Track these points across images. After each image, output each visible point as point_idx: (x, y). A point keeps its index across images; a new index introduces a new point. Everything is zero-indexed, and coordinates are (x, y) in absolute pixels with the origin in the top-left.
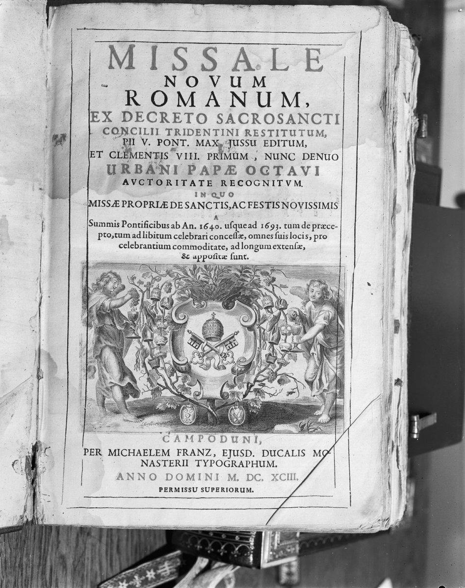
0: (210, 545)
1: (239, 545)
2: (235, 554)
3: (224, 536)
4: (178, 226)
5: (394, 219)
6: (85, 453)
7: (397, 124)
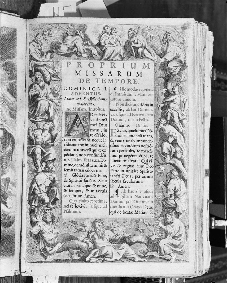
4: (134, 141)
5: (204, 122)
6: (68, 66)
7: (205, 75)
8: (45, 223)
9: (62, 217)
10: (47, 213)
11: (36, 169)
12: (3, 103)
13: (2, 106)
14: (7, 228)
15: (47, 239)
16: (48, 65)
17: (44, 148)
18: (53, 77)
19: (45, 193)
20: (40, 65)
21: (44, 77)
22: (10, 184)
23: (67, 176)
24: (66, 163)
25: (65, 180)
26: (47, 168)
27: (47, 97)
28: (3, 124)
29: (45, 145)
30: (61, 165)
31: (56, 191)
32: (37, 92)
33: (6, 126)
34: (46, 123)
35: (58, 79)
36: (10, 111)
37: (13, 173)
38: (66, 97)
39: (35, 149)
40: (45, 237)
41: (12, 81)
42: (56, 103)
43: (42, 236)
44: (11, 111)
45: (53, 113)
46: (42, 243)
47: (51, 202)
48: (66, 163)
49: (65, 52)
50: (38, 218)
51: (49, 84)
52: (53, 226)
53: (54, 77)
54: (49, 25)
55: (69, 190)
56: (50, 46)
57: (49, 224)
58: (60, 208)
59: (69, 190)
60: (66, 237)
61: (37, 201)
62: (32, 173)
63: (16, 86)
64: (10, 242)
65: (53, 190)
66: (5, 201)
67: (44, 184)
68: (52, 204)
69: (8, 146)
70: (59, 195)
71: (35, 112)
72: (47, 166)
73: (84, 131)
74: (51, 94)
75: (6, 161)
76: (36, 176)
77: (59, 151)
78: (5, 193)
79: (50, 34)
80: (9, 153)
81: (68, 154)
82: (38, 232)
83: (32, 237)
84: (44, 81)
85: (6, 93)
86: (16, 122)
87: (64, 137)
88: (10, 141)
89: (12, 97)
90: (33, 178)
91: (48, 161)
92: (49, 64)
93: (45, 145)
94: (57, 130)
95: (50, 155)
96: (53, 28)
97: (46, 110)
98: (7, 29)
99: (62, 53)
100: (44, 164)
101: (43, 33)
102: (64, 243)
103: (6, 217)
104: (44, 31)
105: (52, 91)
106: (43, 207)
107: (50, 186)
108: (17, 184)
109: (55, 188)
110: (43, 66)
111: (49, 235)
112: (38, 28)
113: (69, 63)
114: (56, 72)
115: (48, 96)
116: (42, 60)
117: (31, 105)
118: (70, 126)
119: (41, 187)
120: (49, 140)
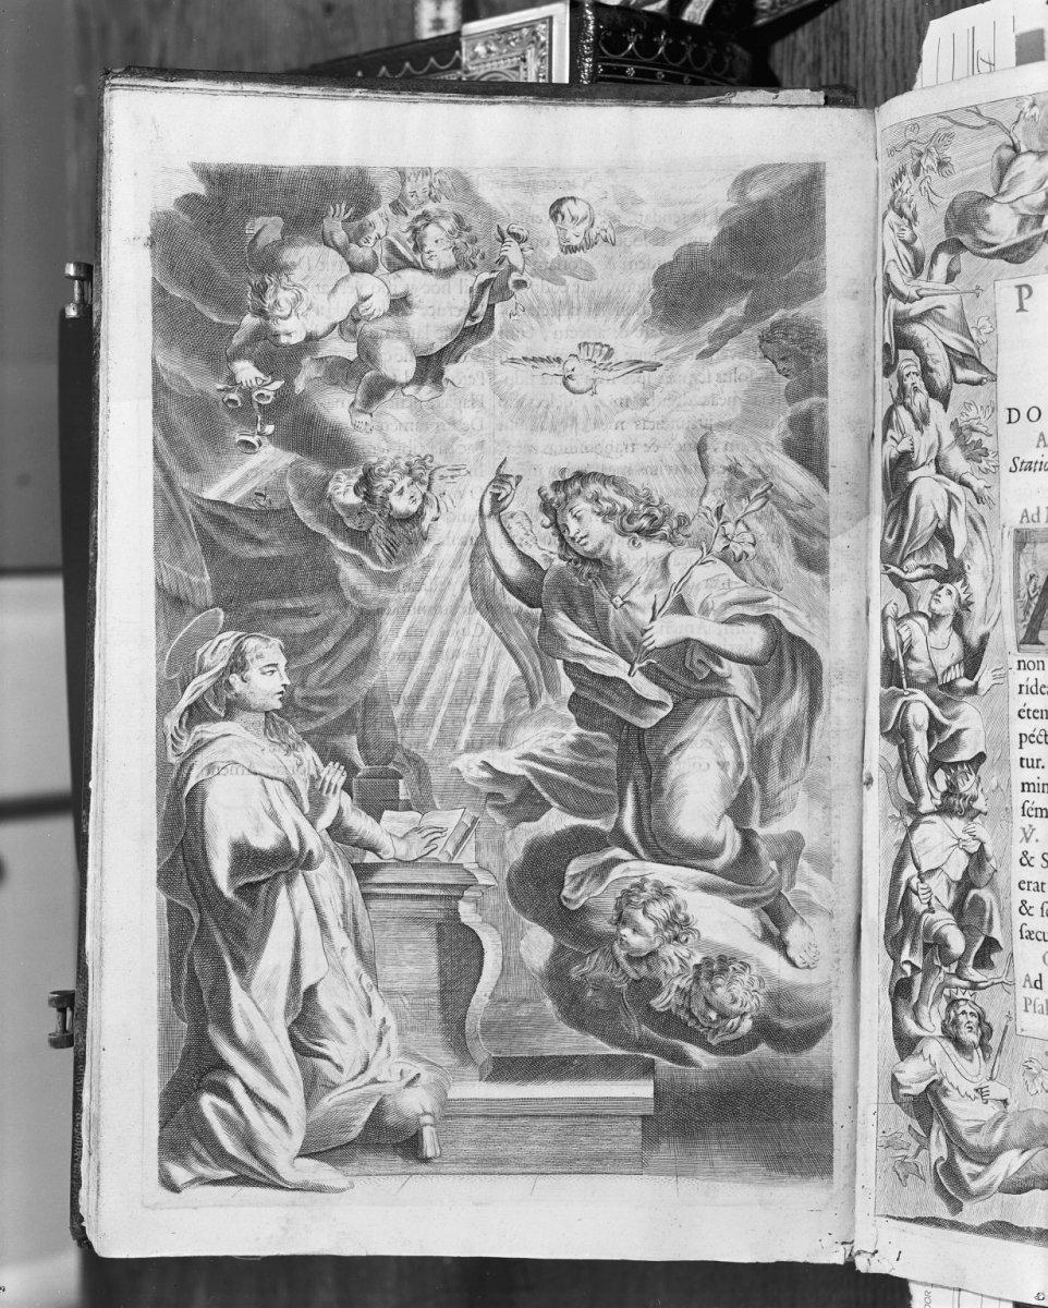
0: (689, 53)
1: (625, 56)
2: (634, 33)
3: (631, 71)
6: (1021, 304)
8: (951, 1046)
9: (1019, 1032)
10: (962, 1003)
11: (910, 799)
12: (762, 507)
13: (759, 519)
14: (794, 1051)
15: (959, 1123)
16: (941, 311)
17: (939, 704)
18: (964, 365)
19: (949, 911)
20: (912, 313)
21: (926, 371)
22: (803, 863)
23: (1033, 839)
24: (1029, 775)
25: (1026, 860)
26: (952, 795)
27: (939, 465)
28: (767, 599)
29: (941, 687)
30: (1009, 785)
31: (988, 906)
32: (905, 446)
33: (778, 608)
34: (940, 589)
35: (980, 376)
36: (796, 542)
37: (818, 813)
38: (1016, 460)
39: (906, 704)
40: (953, 1112)
41: (804, 405)
42: (975, 489)
43: (942, 1109)
44: (803, 538)
45: (965, 540)
46: (937, 1137)
47: (973, 956)
48: (1029, 775)
49: (1006, 238)
50: (925, 1022)
51: (944, 398)
52: (986, 1068)
53: (967, 368)
54: (941, 121)
55: (1023, 808)
56: (946, 219)
57: (969, 1057)
58: (1007, 985)
59: (1023, 808)
60: (1037, 1124)
61: (920, 946)
62: (898, 815)
63: (824, 422)
64: (809, 1116)
65: (976, 898)
66: (780, 937)
67: (944, 867)
68: (975, 966)
69: (791, 693)
70: (1002, 926)
71: (900, 537)
72: (952, 789)
73: (748, 667)
74: (957, 449)
75: (781, 759)
76: (911, 829)
77: (997, 719)
78: (782, 901)
79: (945, 164)
80: (794, 725)
81: (1036, 733)
82: (923, 1086)
83: (900, 1104)
84: (925, 392)
85: (775, 462)
86: (826, 585)
87: (1014, 649)
88: (799, 671)
89: (806, 473)
90: (903, 837)
91: (955, 765)
92: (943, 307)
93: (941, 687)
94: (985, 620)
95: (964, 736)
96: (956, 129)
97: (940, 526)
98: (778, 174)
99: (993, 245)
100: (940, 776)
101: (919, 164)
102: (1034, 1151)
103: (785, 1005)
104: (921, 155)
105: (960, 432)
106: (942, 975)
107: (966, 884)
108: (836, 864)
109: (985, 894)
110: (919, 319)
111: (966, 1104)
112: (901, 141)
113: (1025, 292)
114: (972, 340)
115: (946, 459)
116: (917, 291)
117: (890, 506)
118: (1036, 600)
119: (932, 882)
120: (957, 666)
